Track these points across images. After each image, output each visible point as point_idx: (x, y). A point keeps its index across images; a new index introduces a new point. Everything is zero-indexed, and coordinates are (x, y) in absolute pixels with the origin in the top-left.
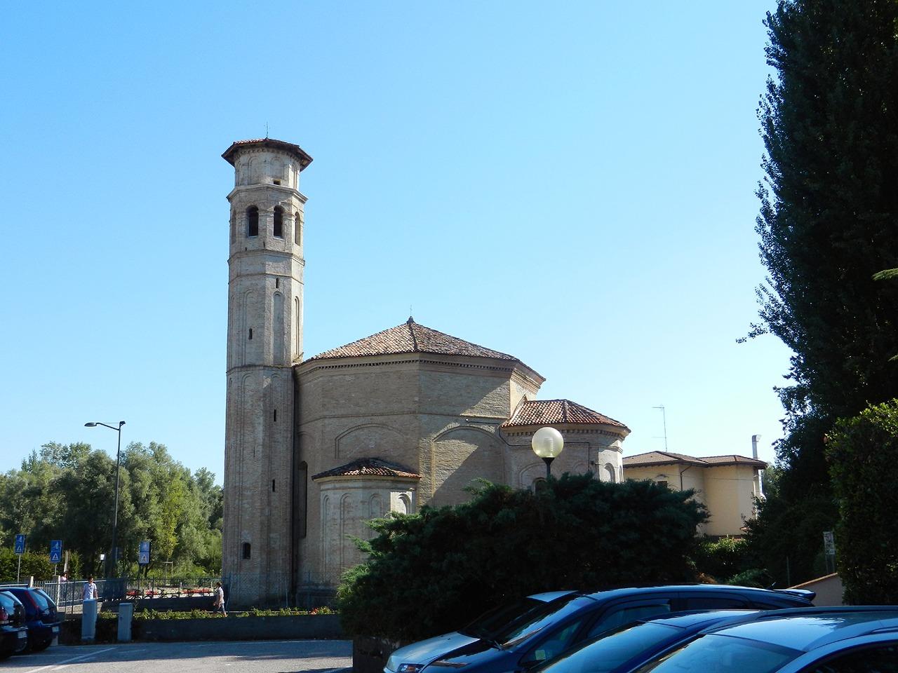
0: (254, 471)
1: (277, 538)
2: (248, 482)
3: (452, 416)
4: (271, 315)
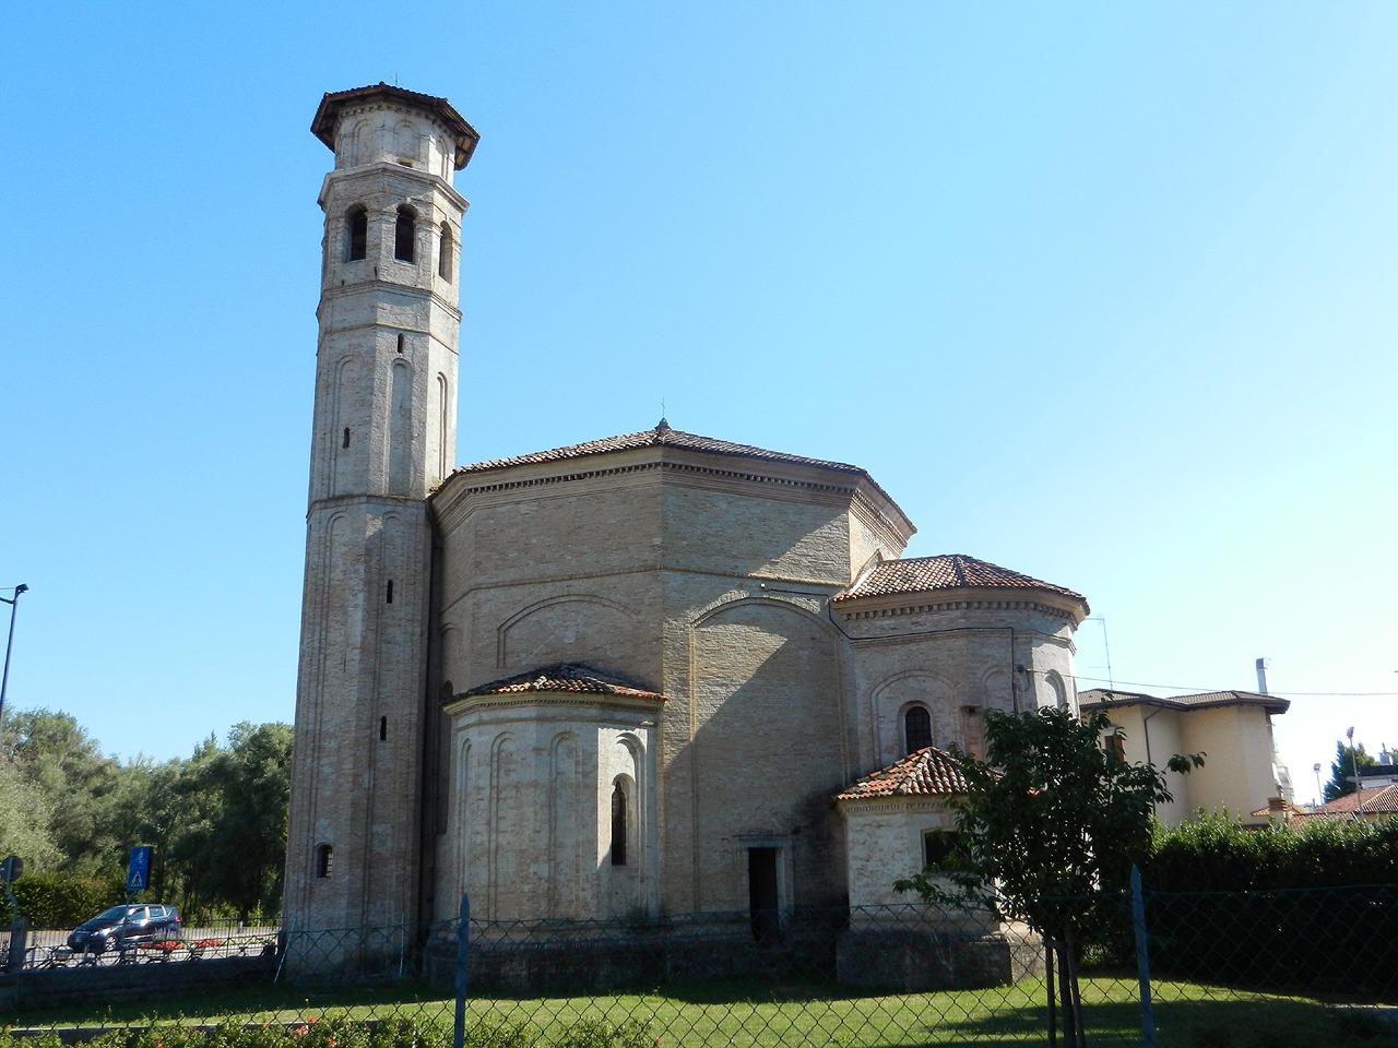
0: (346, 694)
1: (387, 835)
2: (333, 723)
3: (732, 576)
4: (386, 400)
